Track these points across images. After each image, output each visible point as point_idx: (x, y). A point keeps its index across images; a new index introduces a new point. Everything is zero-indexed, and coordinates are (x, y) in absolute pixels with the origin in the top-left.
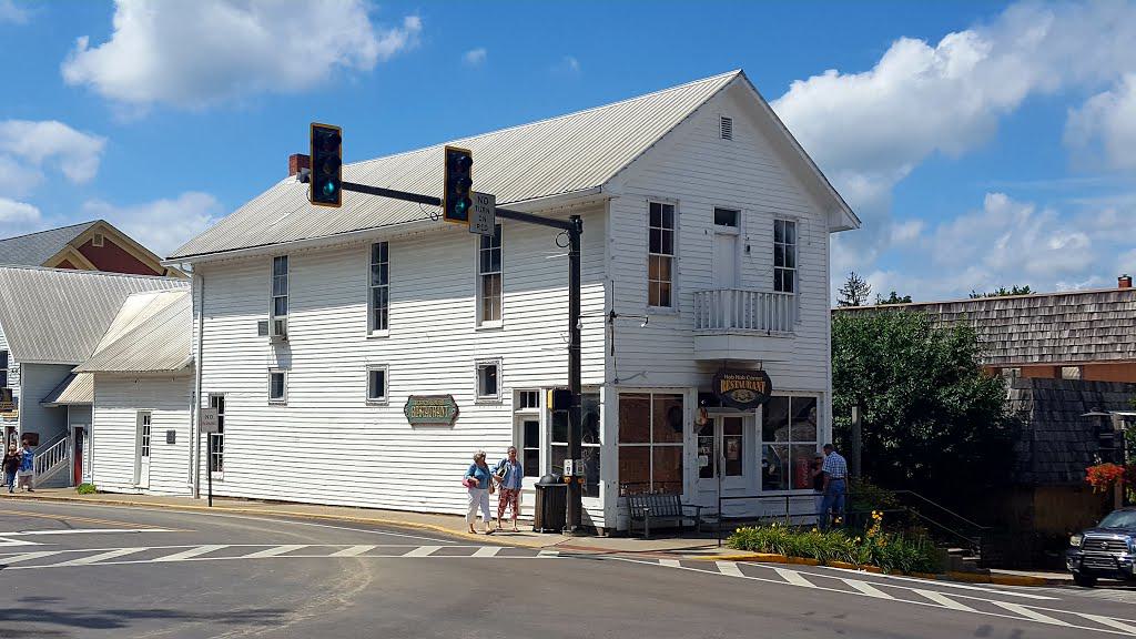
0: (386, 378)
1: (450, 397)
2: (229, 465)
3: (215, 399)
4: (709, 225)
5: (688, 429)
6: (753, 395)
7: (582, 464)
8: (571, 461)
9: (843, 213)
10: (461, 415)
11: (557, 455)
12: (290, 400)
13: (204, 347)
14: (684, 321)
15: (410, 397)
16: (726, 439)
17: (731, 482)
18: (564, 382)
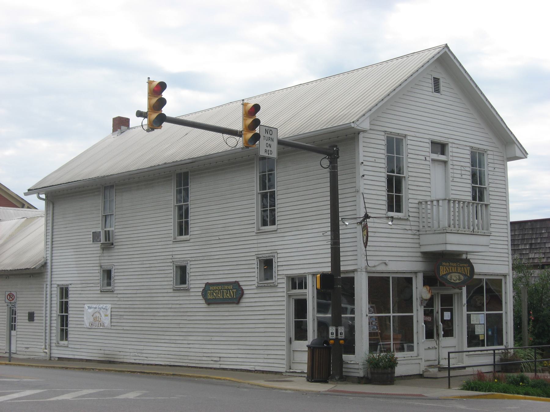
0: (188, 271)
1: (237, 283)
2: (73, 299)
3: (62, 289)
4: (427, 154)
5: (416, 304)
6: (462, 277)
7: (341, 329)
8: (334, 328)
9: (516, 147)
10: (245, 296)
11: (322, 326)
12: (116, 288)
13: (54, 258)
14: (412, 223)
15: (207, 284)
16: (443, 311)
17: (446, 342)
18: (327, 269)
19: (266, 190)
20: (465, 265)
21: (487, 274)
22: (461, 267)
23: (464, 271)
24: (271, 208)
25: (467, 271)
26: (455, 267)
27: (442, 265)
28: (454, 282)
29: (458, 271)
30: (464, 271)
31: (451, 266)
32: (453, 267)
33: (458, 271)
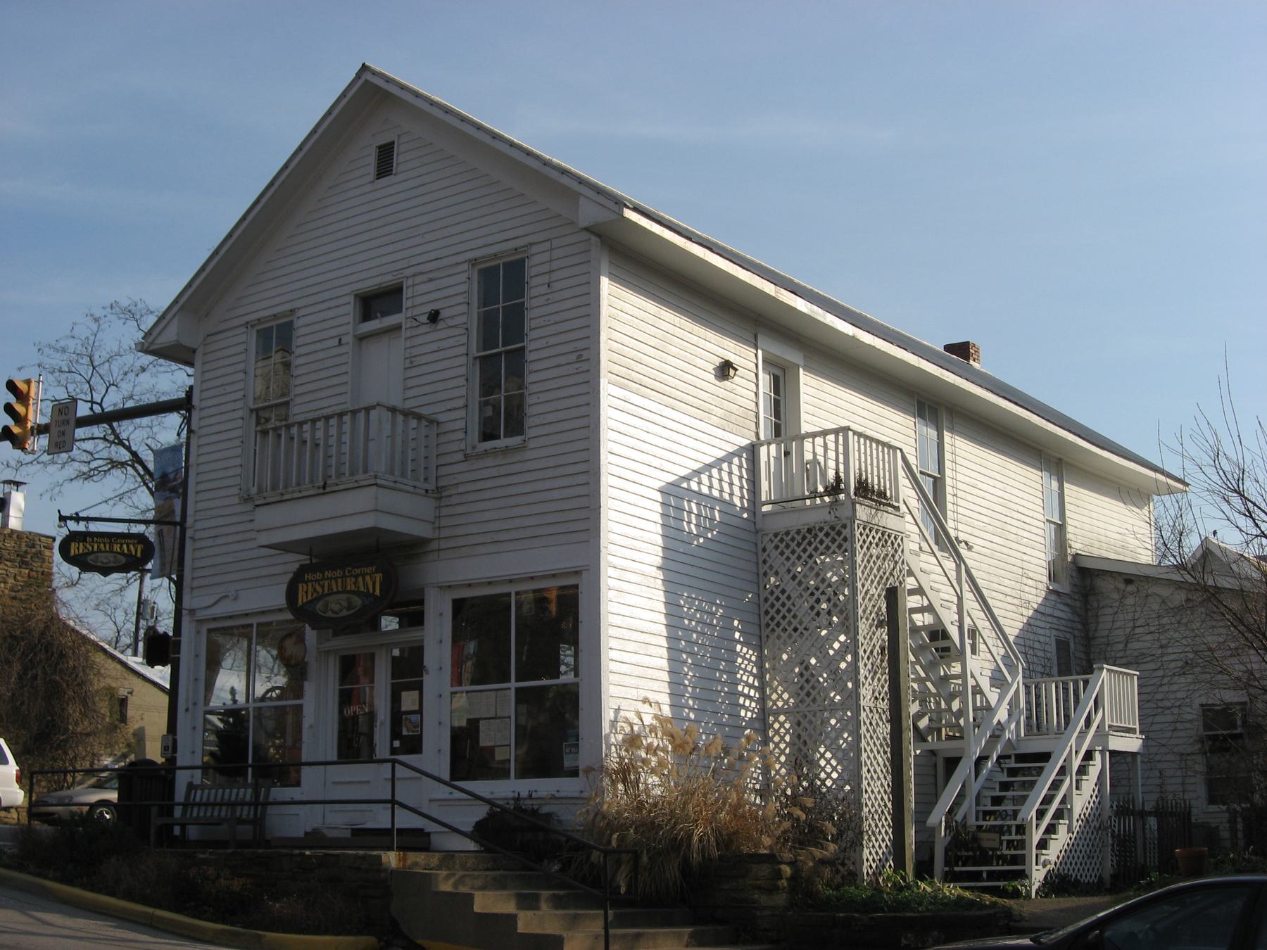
6: (358, 602)
19: (504, 264)
20: (368, 570)
21: (494, 579)
22: (356, 577)
23: (365, 584)
24: (509, 348)
25: (374, 584)
26: (339, 580)
27: (303, 581)
28: (336, 616)
29: (348, 588)
30: (365, 584)
31: (328, 578)
32: (333, 581)
33: (348, 588)
